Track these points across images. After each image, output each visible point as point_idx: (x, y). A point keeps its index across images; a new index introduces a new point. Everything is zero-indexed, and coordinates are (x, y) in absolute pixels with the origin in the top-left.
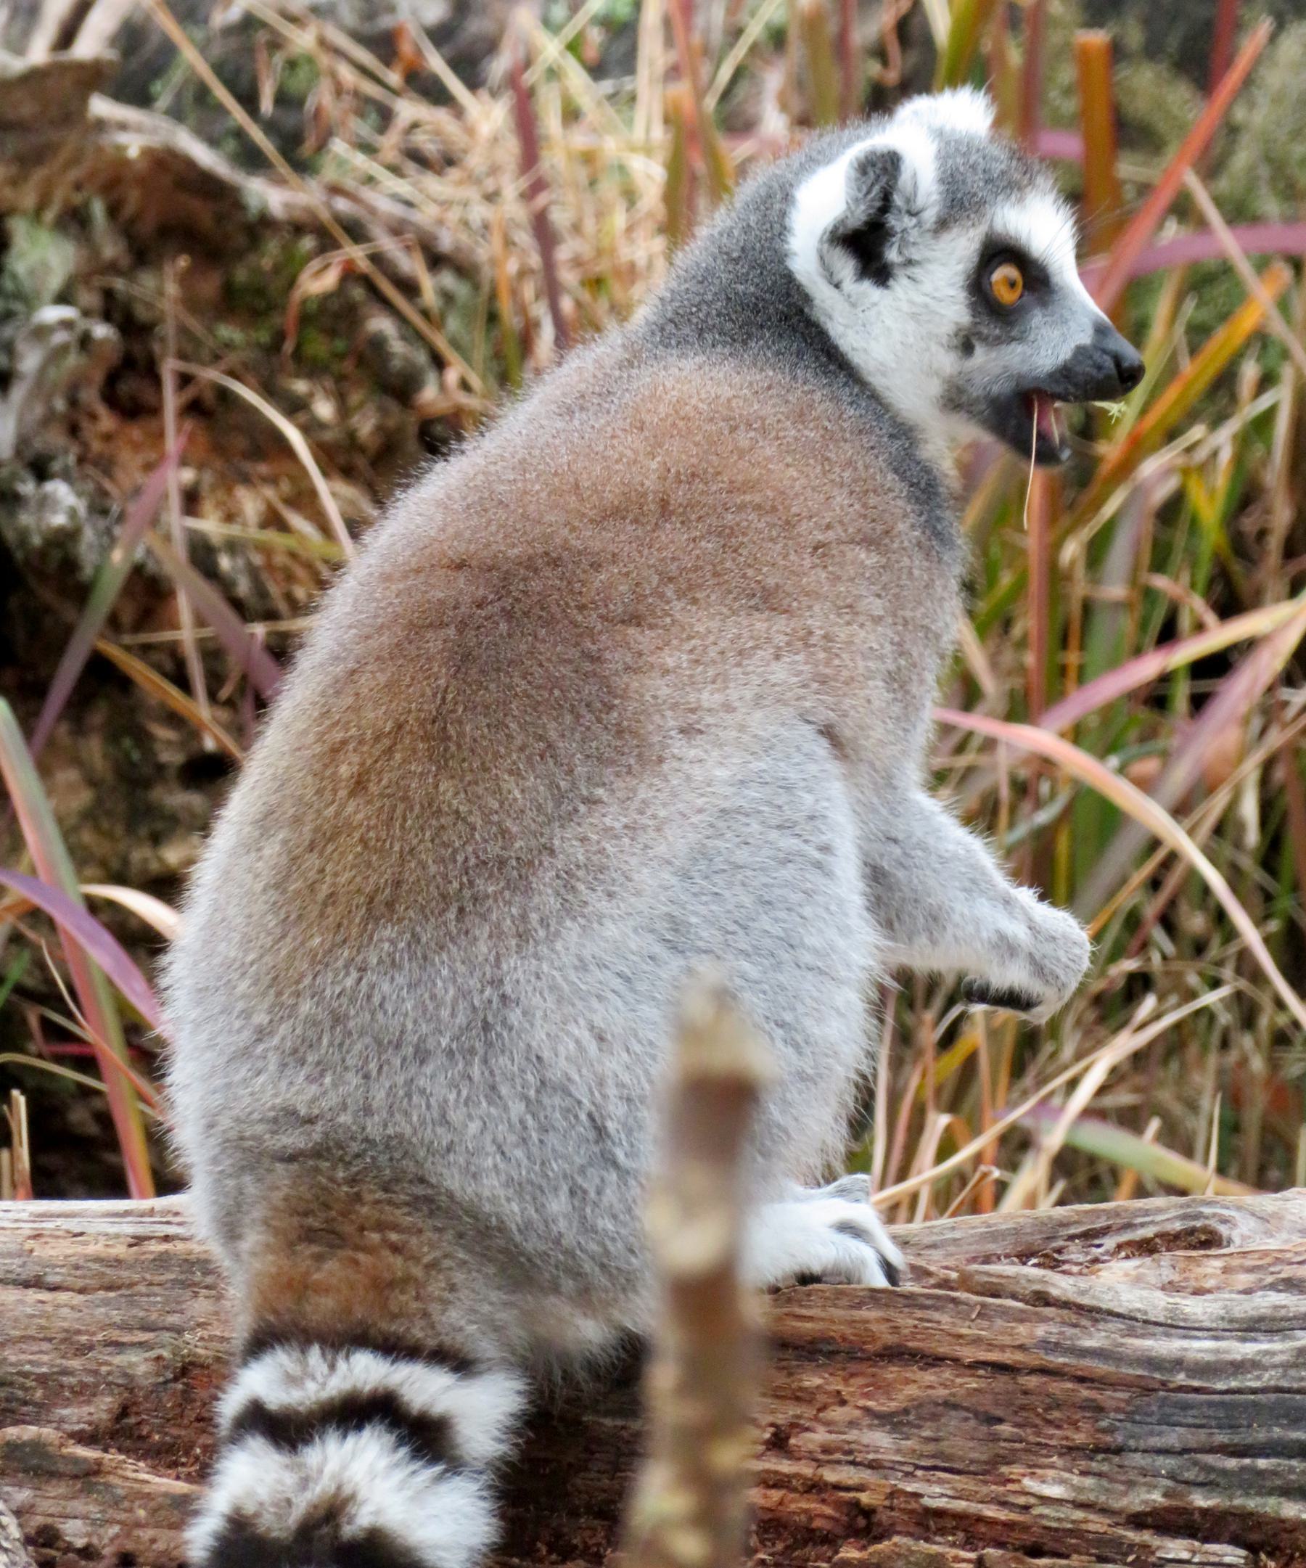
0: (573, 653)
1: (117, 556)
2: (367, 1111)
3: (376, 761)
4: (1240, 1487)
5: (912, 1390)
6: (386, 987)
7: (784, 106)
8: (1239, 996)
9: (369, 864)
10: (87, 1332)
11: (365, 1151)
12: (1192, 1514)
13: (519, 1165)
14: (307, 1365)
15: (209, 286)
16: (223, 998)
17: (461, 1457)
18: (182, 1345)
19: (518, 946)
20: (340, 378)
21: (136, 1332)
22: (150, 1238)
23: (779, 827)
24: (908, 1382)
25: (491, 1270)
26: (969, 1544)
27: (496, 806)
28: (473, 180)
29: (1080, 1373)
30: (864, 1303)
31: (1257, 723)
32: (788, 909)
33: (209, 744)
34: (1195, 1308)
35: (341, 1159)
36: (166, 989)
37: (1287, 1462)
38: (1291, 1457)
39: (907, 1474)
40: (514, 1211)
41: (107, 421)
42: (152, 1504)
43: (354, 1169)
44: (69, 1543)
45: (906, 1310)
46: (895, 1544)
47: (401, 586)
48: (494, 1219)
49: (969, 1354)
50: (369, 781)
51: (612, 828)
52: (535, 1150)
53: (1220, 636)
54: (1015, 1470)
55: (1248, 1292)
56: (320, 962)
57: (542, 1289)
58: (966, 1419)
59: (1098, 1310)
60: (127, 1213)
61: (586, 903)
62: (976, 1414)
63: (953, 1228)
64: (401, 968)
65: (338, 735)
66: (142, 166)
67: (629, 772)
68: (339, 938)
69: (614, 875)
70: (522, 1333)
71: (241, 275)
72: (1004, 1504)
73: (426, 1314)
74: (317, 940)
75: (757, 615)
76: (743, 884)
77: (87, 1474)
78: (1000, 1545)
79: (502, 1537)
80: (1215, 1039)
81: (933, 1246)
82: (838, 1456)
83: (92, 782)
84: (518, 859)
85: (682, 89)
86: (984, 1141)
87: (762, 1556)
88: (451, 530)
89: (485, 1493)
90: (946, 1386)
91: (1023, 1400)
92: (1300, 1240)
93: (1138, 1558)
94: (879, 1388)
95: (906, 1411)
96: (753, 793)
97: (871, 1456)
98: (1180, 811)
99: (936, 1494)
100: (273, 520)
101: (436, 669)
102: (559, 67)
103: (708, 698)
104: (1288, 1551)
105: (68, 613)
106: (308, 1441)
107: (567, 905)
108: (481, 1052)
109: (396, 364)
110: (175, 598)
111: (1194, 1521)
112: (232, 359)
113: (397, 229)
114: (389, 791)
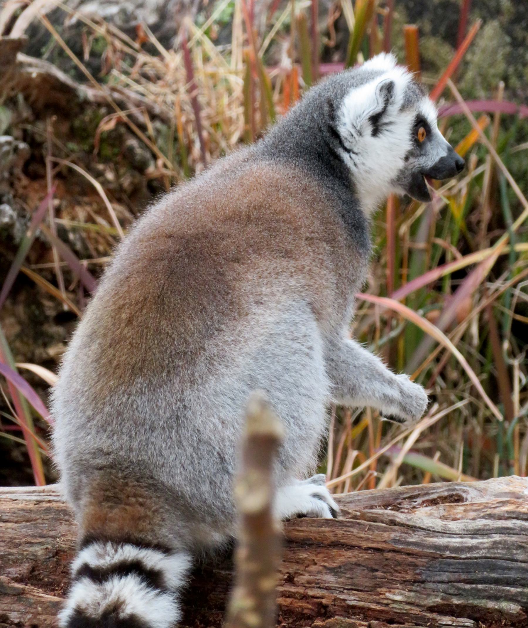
0: (213, 272)
1: (29, 234)
2: (131, 450)
3: (136, 313)
4: (471, 595)
5: (342, 559)
6: (139, 402)
7: (290, 56)
8: (471, 404)
9: (133, 353)
10: (18, 539)
11: (130, 466)
12: (452, 606)
13: (190, 472)
14: (106, 550)
15: (64, 128)
16: (74, 405)
17: (166, 586)
18: (56, 543)
19: (190, 386)
20: (116, 164)
21: (38, 538)
22: (44, 501)
23: (292, 339)
24: (341, 555)
25: (179, 513)
26: (365, 619)
27: (183, 331)
28: (167, 85)
29: (408, 552)
30: (324, 525)
31: (477, 296)
32: (296, 372)
33: (66, 308)
34: (453, 526)
35: (120, 469)
36: (52, 401)
37: (490, 586)
38: (491, 584)
39: (340, 592)
40: (188, 490)
41: (25, 181)
42: (45, 606)
43: (125, 473)
44: (12, 621)
45: (340, 527)
46: (336, 619)
47: (147, 244)
48: (180, 493)
49: (365, 544)
50: (133, 320)
51: (227, 341)
52: (196, 466)
53: (463, 262)
54: (383, 590)
55: (474, 519)
56: (113, 391)
57: (198, 521)
58: (364, 570)
59: (415, 527)
60: (34, 492)
61: (218, 369)
62: (367, 568)
63: (358, 495)
64: (145, 394)
65: (121, 302)
66: (39, 80)
67: (234, 319)
68: (121, 382)
69: (228, 359)
70: (191, 538)
71: (77, 123)
72: (379, 603)
73: (153, 531)
74: (112, 383)
75: (283, 259)
76: (278, 362)
77: (19, 594)
78: (377, 619)
79: (182, 618)
80: (462, 421)
81: (350, 502)
82: (313, 585)
83: (20, 322)
84: (191, 352)
85: (250, 49)
86: (370, 461)
87: (283, 624)
88: (166, 223)
89: (175, 601)
90: (355, 557)
91: (386, 562)
92: (494, 499)
93: (431, 624)
94: (330, 558)
95: (340, 567)
96: (283, 327)
97: (326, 585)
98: (447, 331)
99: (352, 599)
100: (90, 219)
101: (160, 277)
102: (202, 41)
103: (265, 290)
104: (490, 621)
105: (10, 257)
106: (106, 580)
107: (210, 370)
108: (175, 428)
109: (138, 158)
110: (52, 250)
111: (453, 609)
112: (74, 156)
113: (138, 105)
114: (141, 324)
